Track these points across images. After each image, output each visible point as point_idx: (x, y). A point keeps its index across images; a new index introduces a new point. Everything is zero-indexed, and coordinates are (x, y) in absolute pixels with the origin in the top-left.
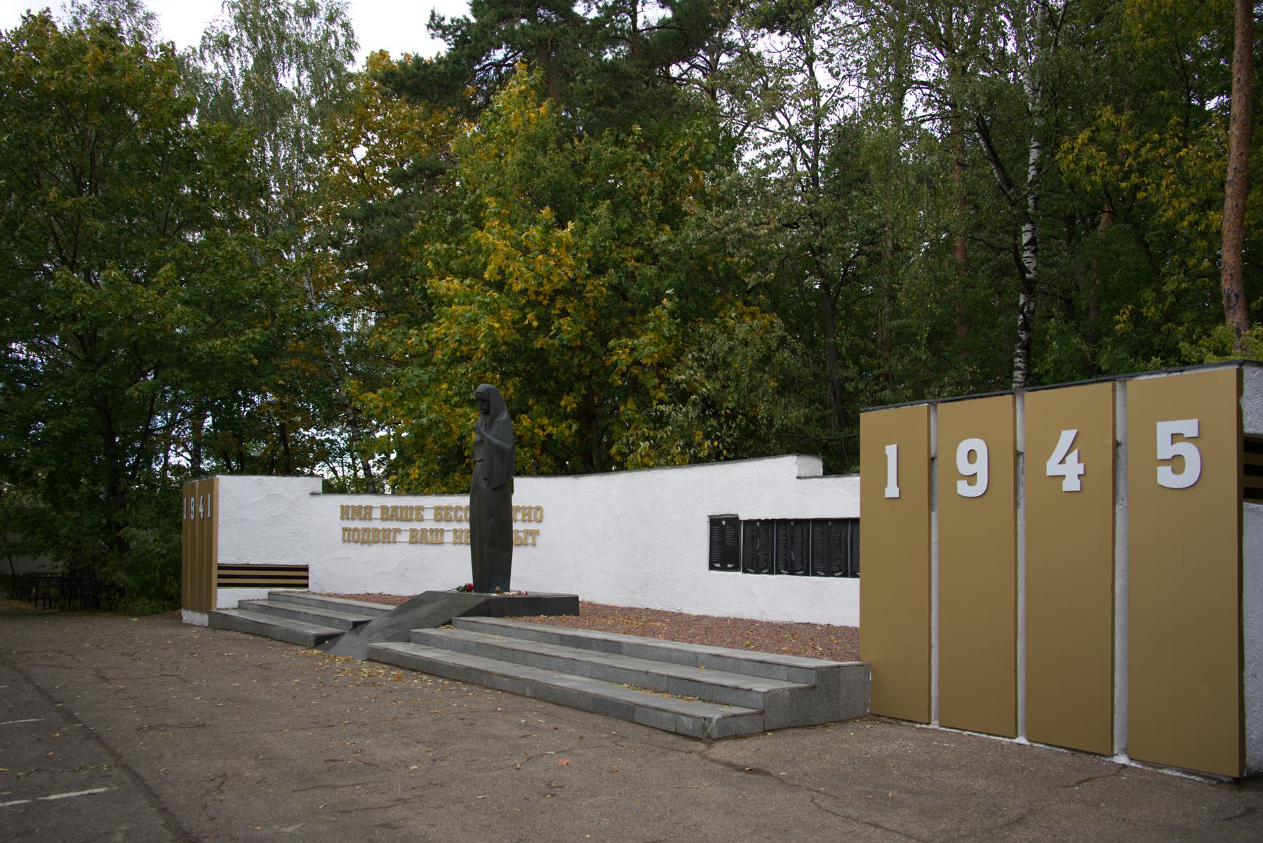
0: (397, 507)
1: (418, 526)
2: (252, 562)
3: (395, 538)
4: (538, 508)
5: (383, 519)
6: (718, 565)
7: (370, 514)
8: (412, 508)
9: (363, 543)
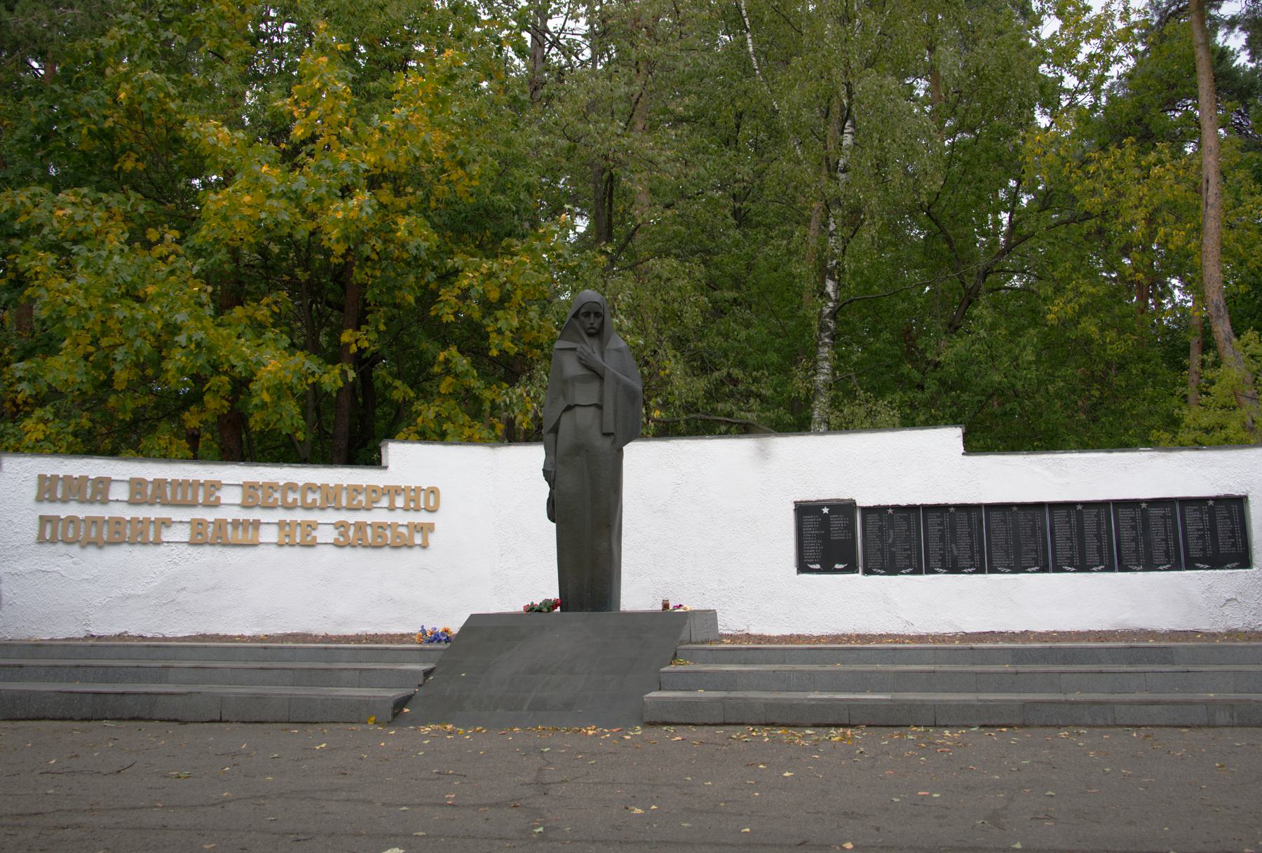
1: (210, 515)
3: (158, 534)
4: (433, 491)
5: (132, 502)
6: (818, 566)
7: (105, 492)
8: (196, 484)
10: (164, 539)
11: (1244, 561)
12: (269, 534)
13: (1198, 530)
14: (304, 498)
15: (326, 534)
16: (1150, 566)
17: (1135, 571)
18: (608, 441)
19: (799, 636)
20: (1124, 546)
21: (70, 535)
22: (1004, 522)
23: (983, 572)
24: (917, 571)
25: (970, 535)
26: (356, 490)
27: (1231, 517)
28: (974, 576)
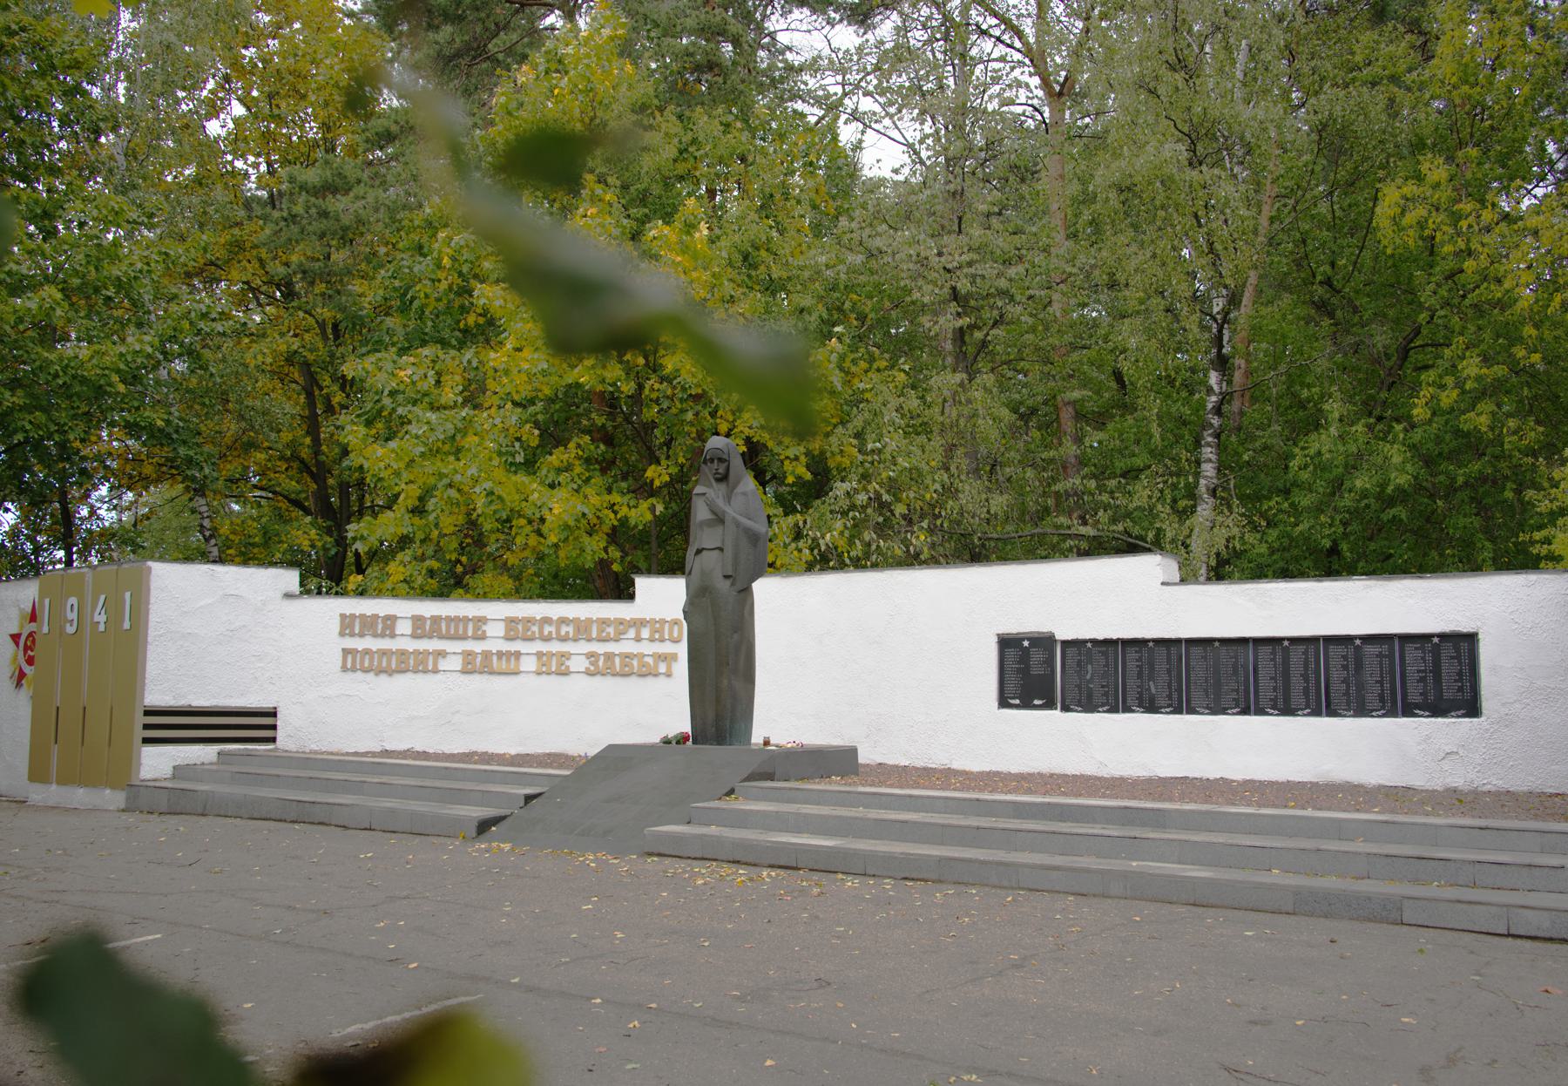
0: (440, 618)
1: (478, 647)
2: (195, 703)
3: (435, 664)
5: (414, 636)
6: (1017, 702)
7: (392, 628)
8: (466, 619)
9: (380, 671)
11: (1471, 708)
12: (529, 664)
13: (1419, 671)
15: (578, 664)
16: (1362, 711)
17: (1345, 716)
18: (728, 582)
19: (927, 772)
20: (1333, 688)
21: (366, 665)
22: (1205, 658)
23: (1180, 712)
24: (1114, 710)
25: (1169, 671)
26: (604, 622)
27: (1458, 657)
28: (1171, 716)
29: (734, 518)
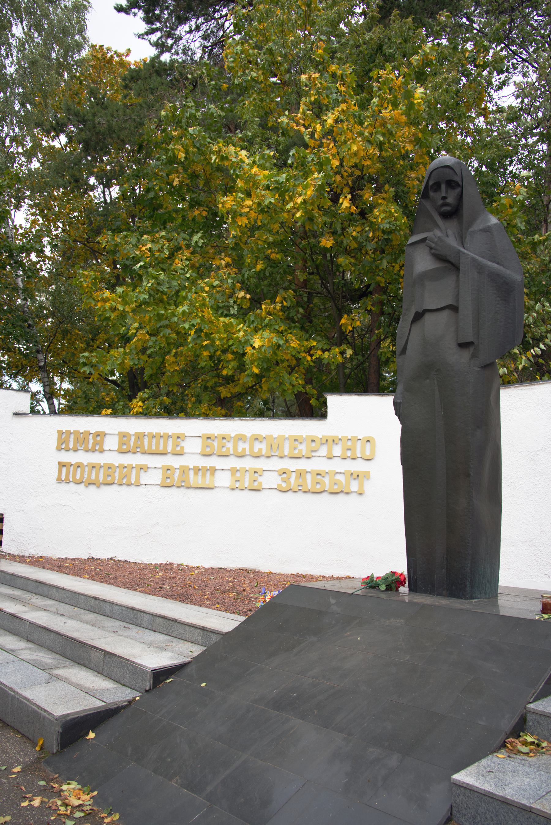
3: (138, 478)
7: (101, 443)
10: (142, 482)
14: (251, 448)
18: (466, 354)
21: (78, 477)
29: (474, 260)
